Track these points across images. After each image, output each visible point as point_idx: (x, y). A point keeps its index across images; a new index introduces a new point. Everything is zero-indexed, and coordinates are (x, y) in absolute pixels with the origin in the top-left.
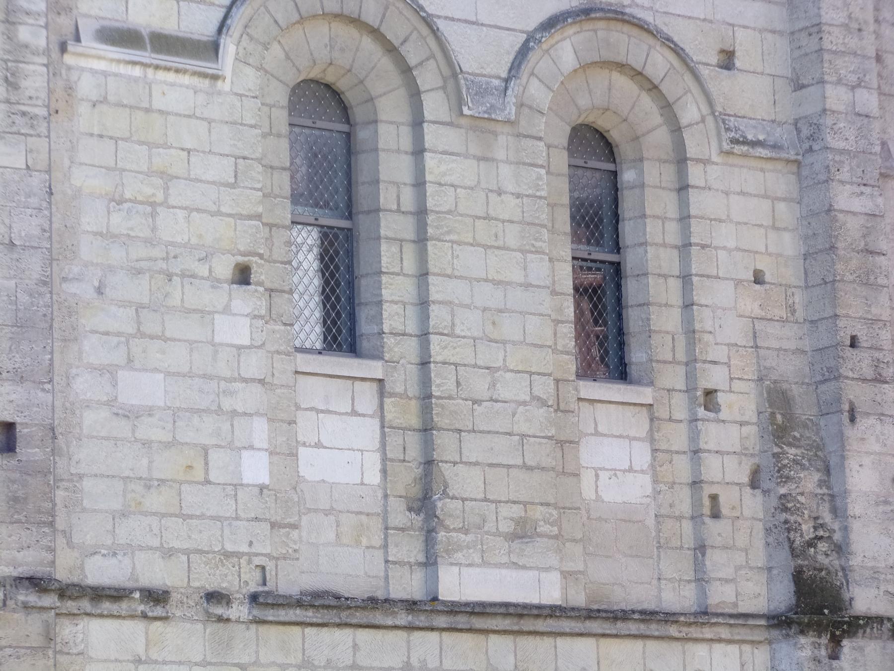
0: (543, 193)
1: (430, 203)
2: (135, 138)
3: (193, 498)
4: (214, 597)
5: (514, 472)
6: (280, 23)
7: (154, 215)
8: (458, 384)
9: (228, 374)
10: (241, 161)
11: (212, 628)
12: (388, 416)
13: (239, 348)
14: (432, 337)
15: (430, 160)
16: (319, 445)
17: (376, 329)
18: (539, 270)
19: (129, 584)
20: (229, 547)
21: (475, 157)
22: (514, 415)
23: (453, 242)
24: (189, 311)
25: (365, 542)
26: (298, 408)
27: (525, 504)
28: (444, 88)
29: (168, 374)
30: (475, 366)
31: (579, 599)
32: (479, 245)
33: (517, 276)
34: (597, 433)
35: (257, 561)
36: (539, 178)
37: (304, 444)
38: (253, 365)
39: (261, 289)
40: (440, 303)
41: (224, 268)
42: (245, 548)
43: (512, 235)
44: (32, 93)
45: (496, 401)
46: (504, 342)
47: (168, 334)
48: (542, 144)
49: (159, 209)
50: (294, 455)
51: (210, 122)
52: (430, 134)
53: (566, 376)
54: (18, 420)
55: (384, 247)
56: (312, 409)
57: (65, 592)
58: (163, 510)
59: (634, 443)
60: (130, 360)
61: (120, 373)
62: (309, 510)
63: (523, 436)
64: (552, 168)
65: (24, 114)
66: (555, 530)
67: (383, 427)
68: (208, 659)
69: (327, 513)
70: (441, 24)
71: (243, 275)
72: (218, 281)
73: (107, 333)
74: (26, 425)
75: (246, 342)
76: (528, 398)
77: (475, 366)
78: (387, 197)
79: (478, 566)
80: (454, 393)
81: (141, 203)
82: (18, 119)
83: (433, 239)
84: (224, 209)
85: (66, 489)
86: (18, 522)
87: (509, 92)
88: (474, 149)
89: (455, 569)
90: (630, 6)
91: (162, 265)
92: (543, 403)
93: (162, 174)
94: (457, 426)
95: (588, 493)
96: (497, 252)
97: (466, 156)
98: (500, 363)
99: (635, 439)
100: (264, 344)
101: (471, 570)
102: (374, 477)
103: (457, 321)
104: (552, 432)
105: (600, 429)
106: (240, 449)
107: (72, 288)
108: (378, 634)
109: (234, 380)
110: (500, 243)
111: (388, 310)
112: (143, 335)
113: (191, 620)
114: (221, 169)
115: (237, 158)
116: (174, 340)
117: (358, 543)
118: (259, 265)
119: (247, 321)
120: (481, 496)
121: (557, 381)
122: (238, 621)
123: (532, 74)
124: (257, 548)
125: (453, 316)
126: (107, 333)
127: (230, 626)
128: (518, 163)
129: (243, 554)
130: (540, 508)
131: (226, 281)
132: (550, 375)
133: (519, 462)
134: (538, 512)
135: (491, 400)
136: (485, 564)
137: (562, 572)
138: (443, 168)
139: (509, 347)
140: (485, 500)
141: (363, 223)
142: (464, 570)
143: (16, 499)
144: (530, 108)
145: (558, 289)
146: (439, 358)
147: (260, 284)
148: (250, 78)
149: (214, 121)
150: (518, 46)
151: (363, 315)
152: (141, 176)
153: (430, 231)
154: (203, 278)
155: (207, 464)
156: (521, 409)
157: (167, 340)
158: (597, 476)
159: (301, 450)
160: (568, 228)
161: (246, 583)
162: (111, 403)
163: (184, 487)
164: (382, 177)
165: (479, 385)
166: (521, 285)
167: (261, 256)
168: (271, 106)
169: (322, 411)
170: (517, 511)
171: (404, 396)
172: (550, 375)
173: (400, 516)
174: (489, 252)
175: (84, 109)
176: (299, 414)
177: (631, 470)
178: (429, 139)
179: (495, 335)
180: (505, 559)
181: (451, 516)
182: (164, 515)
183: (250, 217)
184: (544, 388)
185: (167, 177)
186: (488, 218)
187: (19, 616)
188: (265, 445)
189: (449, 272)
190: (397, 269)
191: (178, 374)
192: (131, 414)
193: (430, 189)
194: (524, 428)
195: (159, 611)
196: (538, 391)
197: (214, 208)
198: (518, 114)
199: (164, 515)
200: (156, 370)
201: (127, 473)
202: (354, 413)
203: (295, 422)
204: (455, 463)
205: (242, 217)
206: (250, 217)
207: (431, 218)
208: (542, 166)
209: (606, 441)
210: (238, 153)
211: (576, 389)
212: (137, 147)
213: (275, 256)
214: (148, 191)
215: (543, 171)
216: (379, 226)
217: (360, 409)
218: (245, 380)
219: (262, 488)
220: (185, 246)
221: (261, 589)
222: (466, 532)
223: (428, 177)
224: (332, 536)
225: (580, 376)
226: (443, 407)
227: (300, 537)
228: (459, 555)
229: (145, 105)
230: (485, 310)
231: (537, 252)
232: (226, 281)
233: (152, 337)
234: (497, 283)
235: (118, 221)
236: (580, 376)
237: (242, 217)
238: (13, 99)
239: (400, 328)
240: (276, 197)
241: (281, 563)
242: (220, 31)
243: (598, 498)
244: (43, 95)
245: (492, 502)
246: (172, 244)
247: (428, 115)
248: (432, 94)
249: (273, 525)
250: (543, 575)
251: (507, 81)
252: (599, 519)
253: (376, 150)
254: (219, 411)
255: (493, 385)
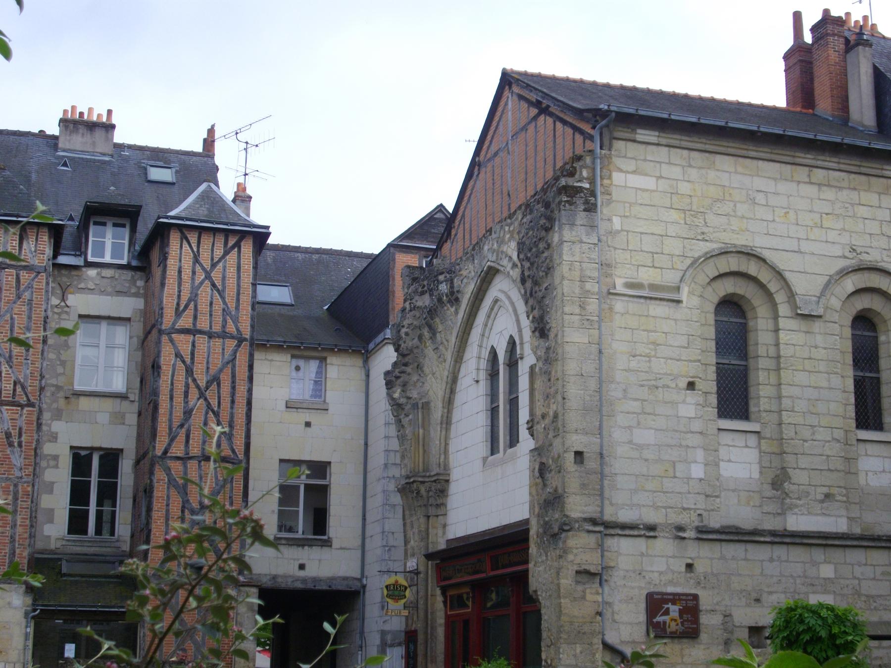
0: (838, 347)
1: (782, 353)
2: (642, 328)
3: (668, 484)
4: (680, 528)
5: (824, 473)
6: (598, 581)
7: (650, 361)
8: (796, 433)
9: (684, 430)
10: (690, 337)
11: (677, 541)
12: (763, 448)
13: (690, 418)
14: (783, 413)
15: (782, 334)
16: (729, 461)
17: (757, 409)
18: (836, 381)
19: (639, 522)
20: (685, 506)
21: (804, 332)
22: (824, 446)
23: (793, 370)
24: (666, 403)
25: (752, 504)
26: (719, 444)
27: (829, 486)
28: (788, 302)
29: (656, 430)
30: (804, 425)
31: (857, 530)
32: (806, 371)
33: (825, 384)
34: (867, 455)
35: (699, 512)
36: (836, 340)
37: (722, 460)
38: (697, 426)
39: (700, 392)
40: (787, 397)
41: (683, 383)
42: (693, 506)
43: (822, 367)
44: (592, 311)
45: (815, 440)
46: (818, 414)
47: (656, 413)
48: (837, 325)
49: (652, 359)
50: (717, 465)
51: (675, 320)
52: (782, 323)
53: (851, 429)
54: (585, 450)
55: (760, 373)
56: (726, 445)
57: (607, 525)
58: (654, 489)
59: (885, 459)
60: (639, 423)
61: (634, 430)
62: (725, 490)
63: (828, 456)
64: (844, 336)
65: (588, 320)
66: (845, 499)
67: (760, 453)
68: (676, 555)
69: (734, 491)
70: (787, 275)
71: (691, 386)
72: (680, 389)
73: (628, 413)
74: (588, 453)
75: (693, 415)
76: (830, 439)
77: (804, 425)
78: (762, 351)
79: (806, 515)
80: (794, 437)
81: (644, 356)
82: (585, 322)
83: (784, 368)
84: (682, 358)
85: (609, 480)
86: (585, 494)
87: (820, 303)
88: (803, 328)
89: (795, 516)
90: (880, 262)
91: (653, 383)
92: (838, 441)
93: (654, 343)
94: (796, 452)
95: (862, 482)
96: (815, 374)
97: (799, 331)
98: (817, 424)
99: (886, 457)
100: (702, 416)
101: (803, 517)
102: (756, 475)
103: (795, 405)
104: (843, 454)
105: (868, 453)
106: (690, 463)
107: (612, 394)
108: (757, 546)
109: (688, 432)
110: (817, 370)
111: (763, 401)
112: (645, 413)
113: (667, 538)
114: (682, 341)
115: (689, 335)
116: (659, 415)
117: (748, 504)
118: (699, 382)
119: (694, 407)
120: (808, 483)
121: (846, 431)
122: (689, 539)
123: (832, 294)
124: (699, 506)
125: (793, 402)
126: (628, 413)
127: (686, 541)
128: (826, 334)
129: (692, 509)
130: (837, 489)
131: (684, 389)
132: (842, 428)
133: (826, 468)
134: (835, 491)
135: (813, 440)
136: (809, 513)
137: (848, 518)
138: (788, 337)
139: (821, 416)
140: (810, 485)
141: (751, 362)
142: (799, 517)
143: (584, 484)
144: (831, 309)
145: (846, 390)
146: (787, 422)
147: (699, 390)
148: (696, 301)
149: (678, 320)
150: (824, 283)
151: (752, 403)
152: (644, 345)
153: (782, 365)
154: (673, 388)
155: (674, 469)
156: (827, 444)
157: (655, 415)
158: (867, 474)
159: (722, 464)
160: (851, 363)
161: (693, 522)
162: (630, 442)
163: (664, 479)
164: (760, 342)
165: (806, 433)
166: (827, 388)
167: (700, 378)
168: (706, 313)
169: (731, 446)
170: (825, 490)
171: (771, 439)
172: (842, 428)
173: (769, 492)
174: (811, 374)
175: (617, 317)
176: (720, 447)
177: (884, 471)
178: (781, 325)
179: (814, 411)
180: (819, 512)
181: (792, 492)
182: (655, 492)
183: (695, 361)
184: (839, 434)
185: (655, 344)
186: (810, 358)
187: (585, 535)
188: (703, 461)
189: (791, 383)
190: (767, 383)
191: (661, 430)
192: (640, 447)
193: (782, 347)
194: (829, 453)
195: (652, 534)
196: (836, 436)
197: (678, 358)
198: (825, 312)
199: (655, 492)
200: (651, 428)
201: (638, 473)
202: (747, 446)
203: (718, 451)
204: (794, 469)
205: (690, 361)
206: (695, 361)
207: (782, 360)
208: (837, 335)
209: (871, 458)
210: (689, 333)
211: (856, 435)
212: (642, 333)
213: (708, 378)
214: (648, 351)
215: (838, 338)
216: (758, 364)
217: (749, 444)
218: (692, 432)
219: (701, 480)
220: (664, 374)
221: (701, 524)
222: (800, 500)
223: (781, 341)
224: (736, 501)
225: (857, 427)
226: (788, 443)
227: (721, 502)
228: (796, 510)
229: (646, 314)
230: (809, 400)
231: (835, 374)
232: (684, 389)
233: (649, 414)
234: (815, 388)
235: (634, 364)
236: (857, 427)
237: (690, 361)
238: (583, 314)
239: (767, 407)
240: (709, 352)
241: (711, 513)
242: (681, 281)
243: (867, 484)
244: (597, 312)
245: (813, 486)
246: (659, 374)
247: (780, 314)
248: (782, 305)
249: (707, 496)
250: (839, 519)
251: (819, 298)
252: (868, 494)
253: (757, 330)
254: (681, 446)
255: (813, 434)
